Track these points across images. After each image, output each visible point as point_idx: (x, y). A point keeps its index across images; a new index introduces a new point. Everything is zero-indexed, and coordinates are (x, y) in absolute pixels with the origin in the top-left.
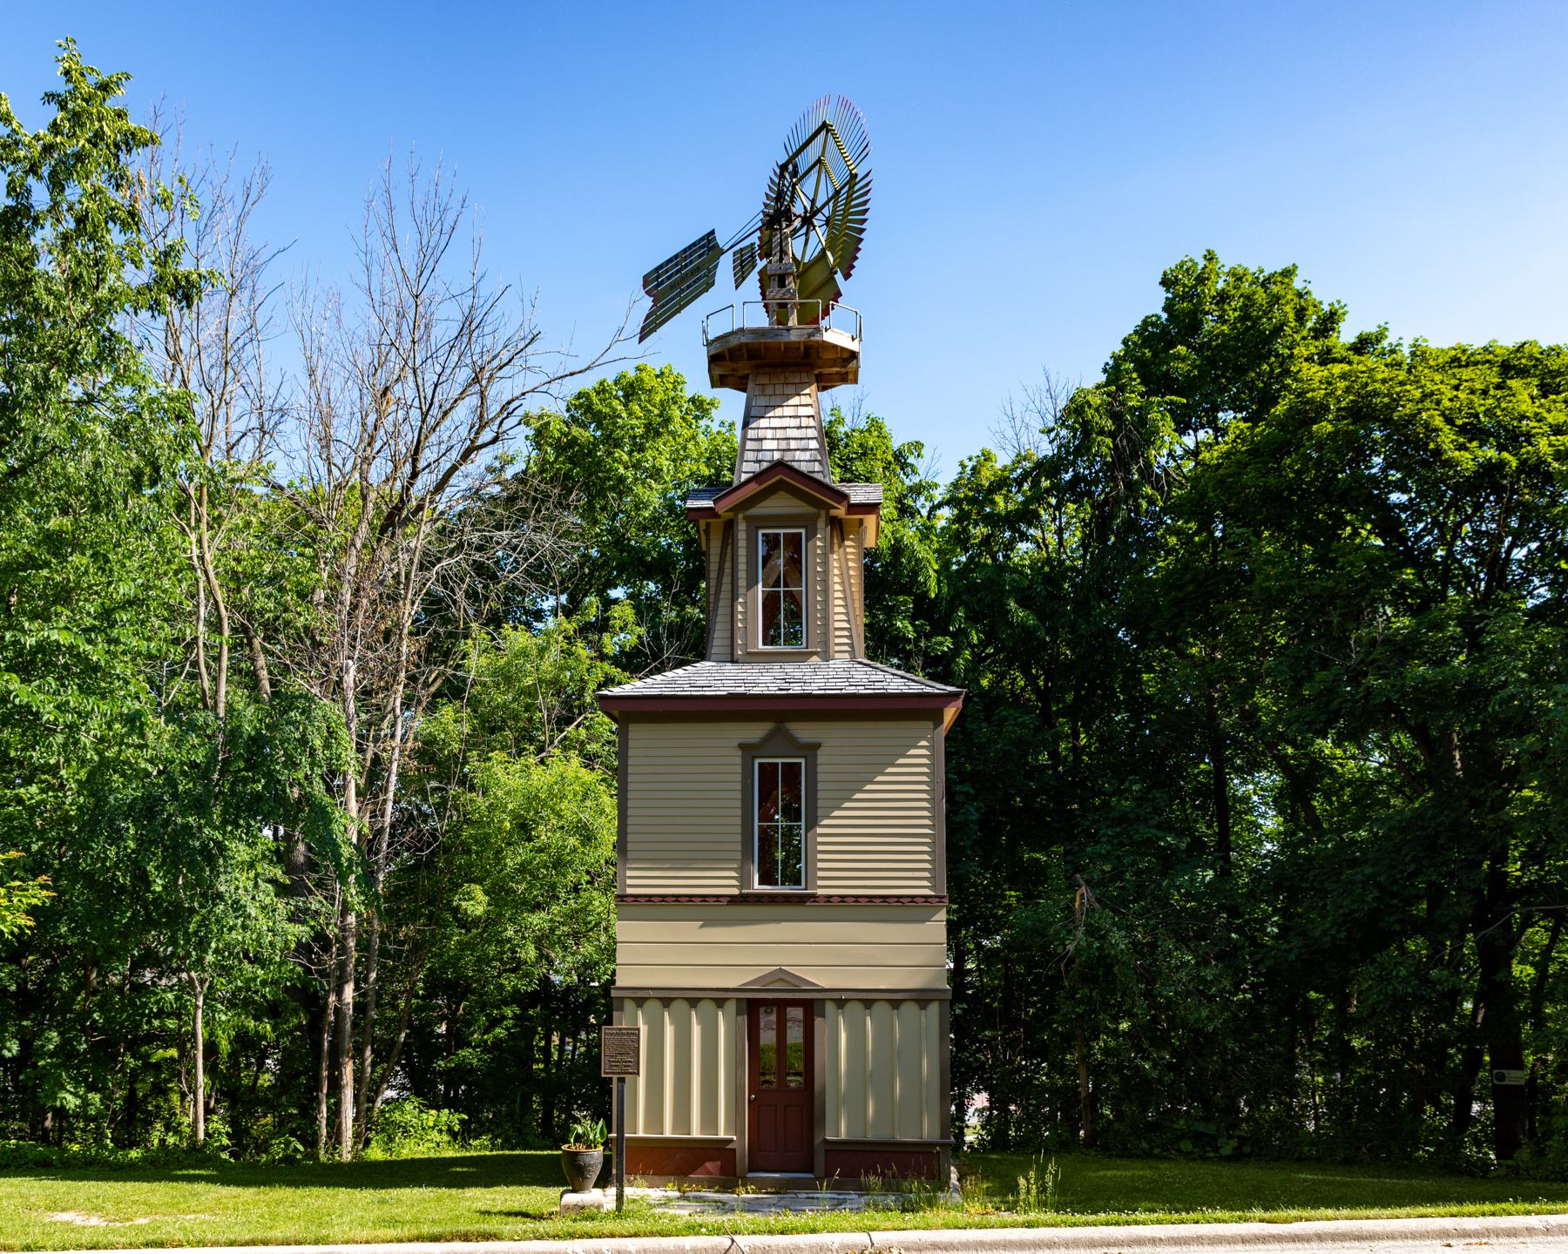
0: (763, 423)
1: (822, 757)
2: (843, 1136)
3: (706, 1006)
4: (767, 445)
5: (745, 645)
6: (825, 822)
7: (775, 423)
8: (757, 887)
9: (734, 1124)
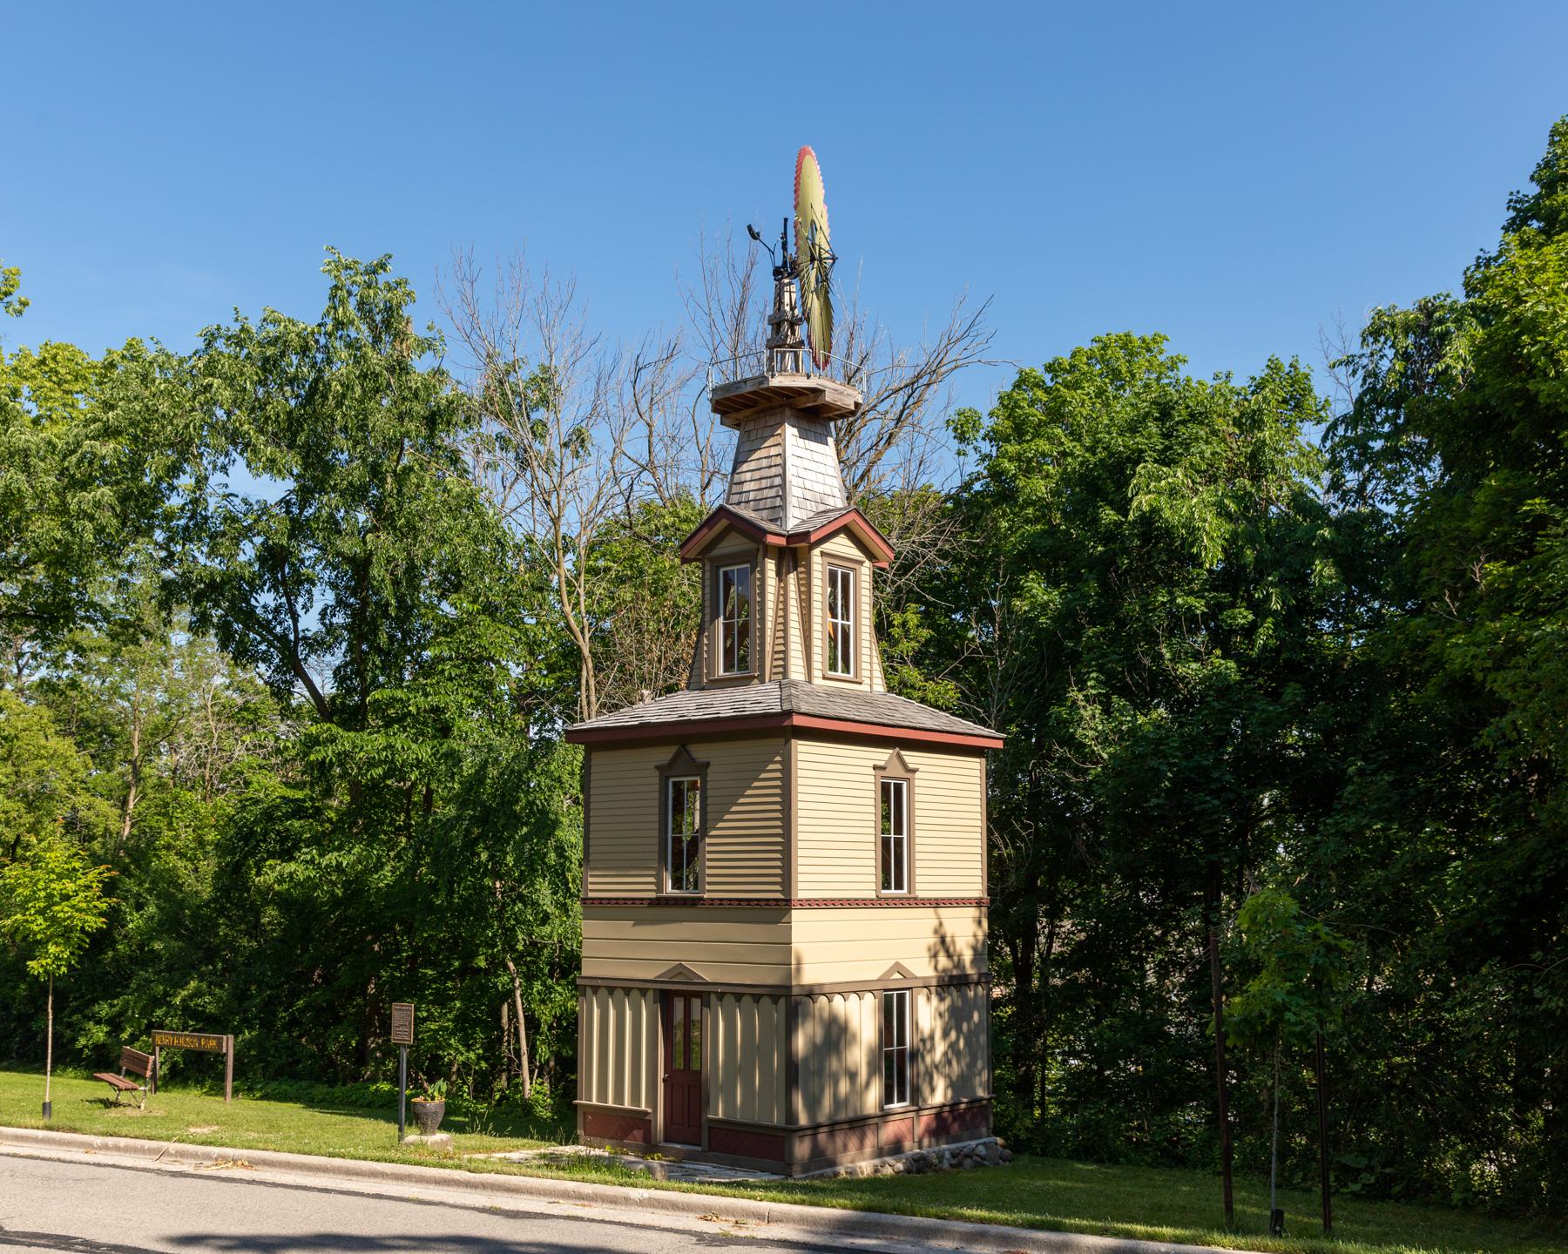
0: (745, 467)
1: (711, 774)
2: (720, 1116)
3: (619, 993)
4: (746, 487)
5: (708, 674)
6: (713, 833)
7: (752, 465)
8: (669, 889)
9: (652, 1100)
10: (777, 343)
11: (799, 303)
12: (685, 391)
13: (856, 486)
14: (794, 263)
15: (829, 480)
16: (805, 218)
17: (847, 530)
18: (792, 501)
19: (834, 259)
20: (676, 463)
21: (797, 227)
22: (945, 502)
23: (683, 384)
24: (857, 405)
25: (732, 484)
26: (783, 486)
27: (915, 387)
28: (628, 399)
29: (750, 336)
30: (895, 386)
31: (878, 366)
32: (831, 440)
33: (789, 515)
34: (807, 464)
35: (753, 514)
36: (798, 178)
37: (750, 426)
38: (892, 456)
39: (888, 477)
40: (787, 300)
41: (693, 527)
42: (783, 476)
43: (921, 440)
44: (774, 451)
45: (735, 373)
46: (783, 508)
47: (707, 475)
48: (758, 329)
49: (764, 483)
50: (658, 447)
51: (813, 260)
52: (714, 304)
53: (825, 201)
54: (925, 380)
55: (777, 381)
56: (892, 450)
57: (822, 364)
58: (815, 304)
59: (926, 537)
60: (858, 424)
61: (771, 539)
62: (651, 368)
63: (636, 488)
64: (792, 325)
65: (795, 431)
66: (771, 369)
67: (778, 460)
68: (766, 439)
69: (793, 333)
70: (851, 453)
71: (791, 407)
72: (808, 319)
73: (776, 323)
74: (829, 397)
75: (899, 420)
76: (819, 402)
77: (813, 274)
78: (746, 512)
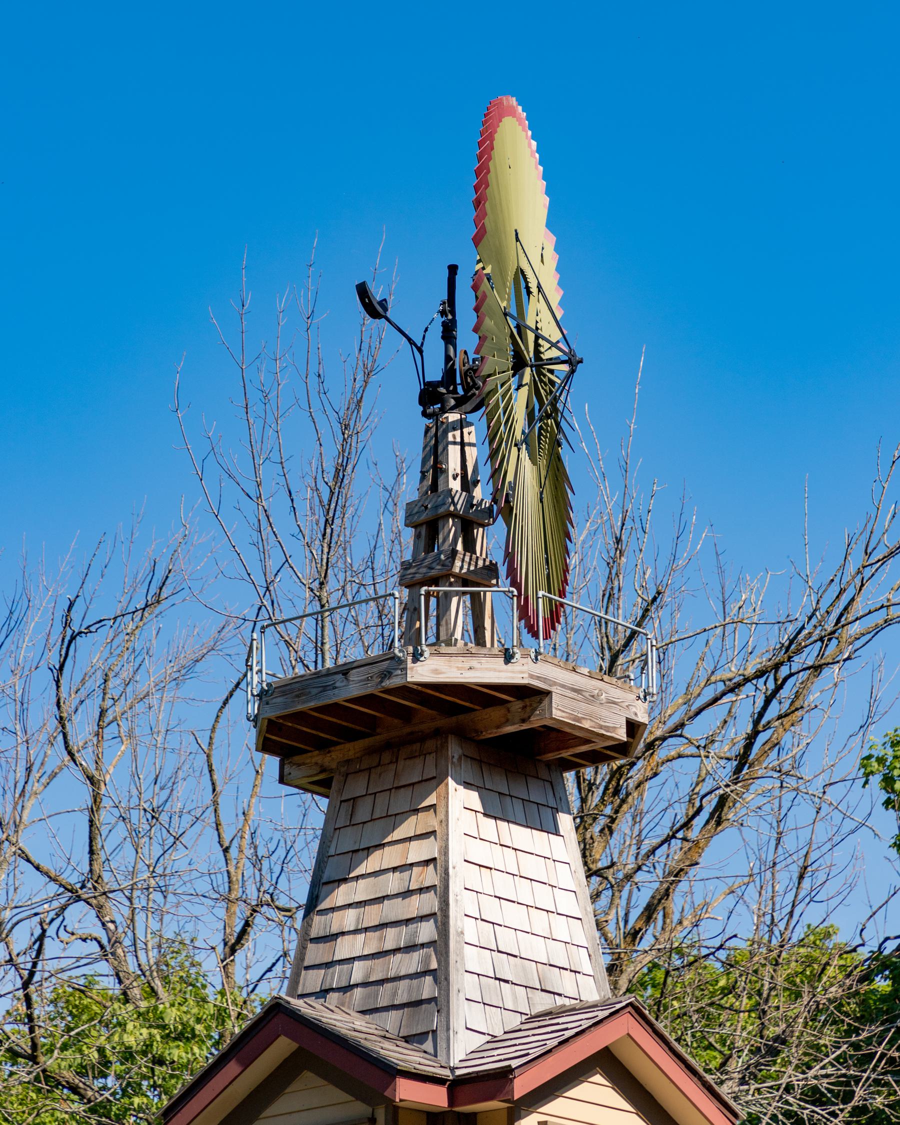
0: (342, 895)
4: (345, 948)
10: (427, 575)
11: (485, 473)
12: (190, 688)
13: (634, 935)
14: (472, 372)
15: (561, 928)
16: (499, 260)
17: (609, 1064)
18: (463, 987)
19: (573, 362)
20: (161, 884)
21: (476, 284)
22: (867, 978)
23: (185, 672)
24: (633, 727)
25: (306, 939)
26: (441, 945)
27: (781, 676)
28: (42, 714)
29: (358, 554)
30: (732, 671)
31: (686, 624)
32: (565, 821)
33: (457, 1023)
34: (504, 886)
35: (360, 1023)
36: (482, 172)
37: (357, 787)
38: (727, 853)
39: (719, 909)
40: (453, 463)
41: (201, 1055)
42: (441, 918)
43: (803, 812)
44: (418, 851)
45: (319, 648)
46: (440, 1003)
47: (241, 911)
48: (380, 534)
49: (392, 938)
50: (113, 838)
51: (519, 364)
52: (269, 473)
53: (551, 224)
54: (808, 657)
55: (427, 670)
56: (727, 837)
57: (541, 622)
58: (526, 474)
59: (821, 1074)
60: (636, 773)
61: (407, 1092)
62: (105, 633)
63: (51, 948)
64: (467, 527)
65: (473, 798)
66: (412, 637)
67: (430, 876)
68: (396, 819)
69: (469, 546)
70: (619, 849)
71: (463, 735)
72: (508, 512)
73: (427, 525)
74: (561, 710)
75: (743, 760)
76: (536, 722)
77: (520, 400)
78: (341, 1018)
